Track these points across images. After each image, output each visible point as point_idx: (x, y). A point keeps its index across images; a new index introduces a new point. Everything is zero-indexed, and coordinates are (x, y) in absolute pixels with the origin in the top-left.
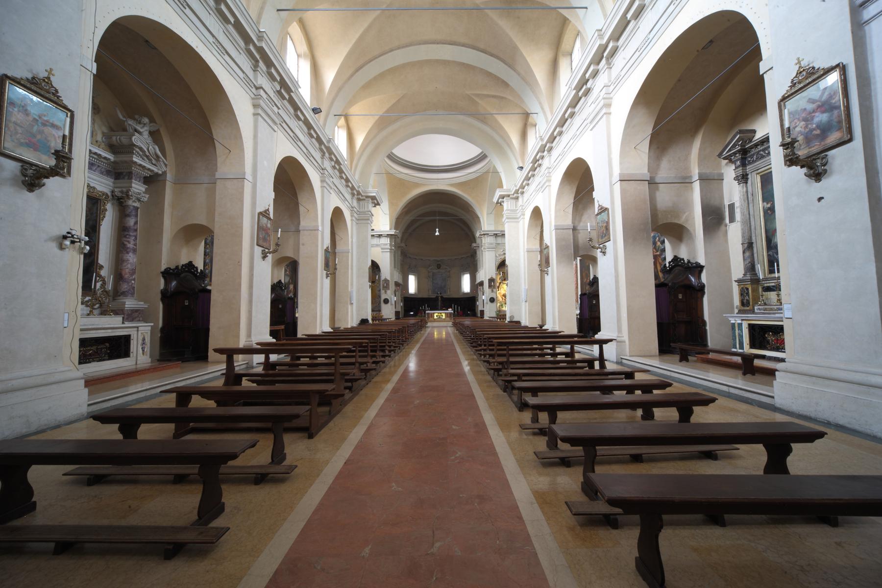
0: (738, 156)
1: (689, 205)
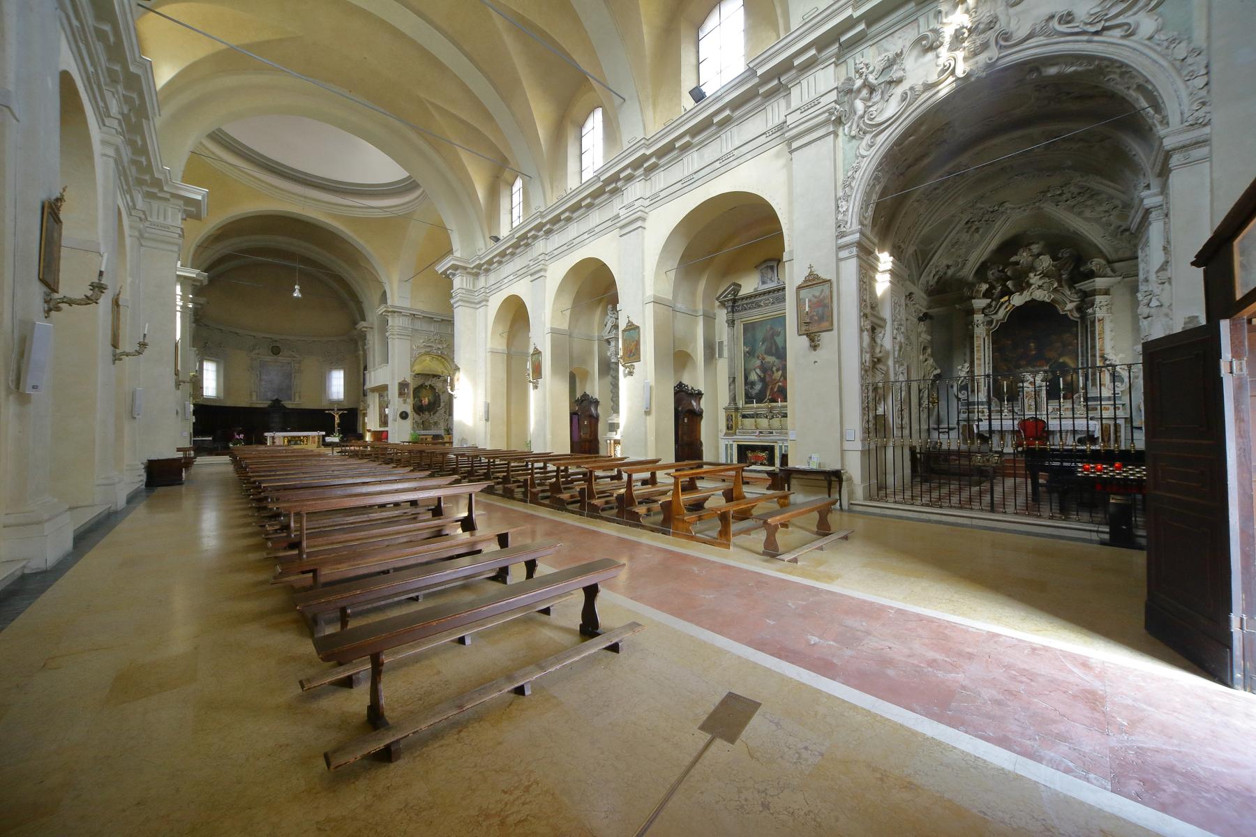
0: (730, 304)
1: (694, 339)
